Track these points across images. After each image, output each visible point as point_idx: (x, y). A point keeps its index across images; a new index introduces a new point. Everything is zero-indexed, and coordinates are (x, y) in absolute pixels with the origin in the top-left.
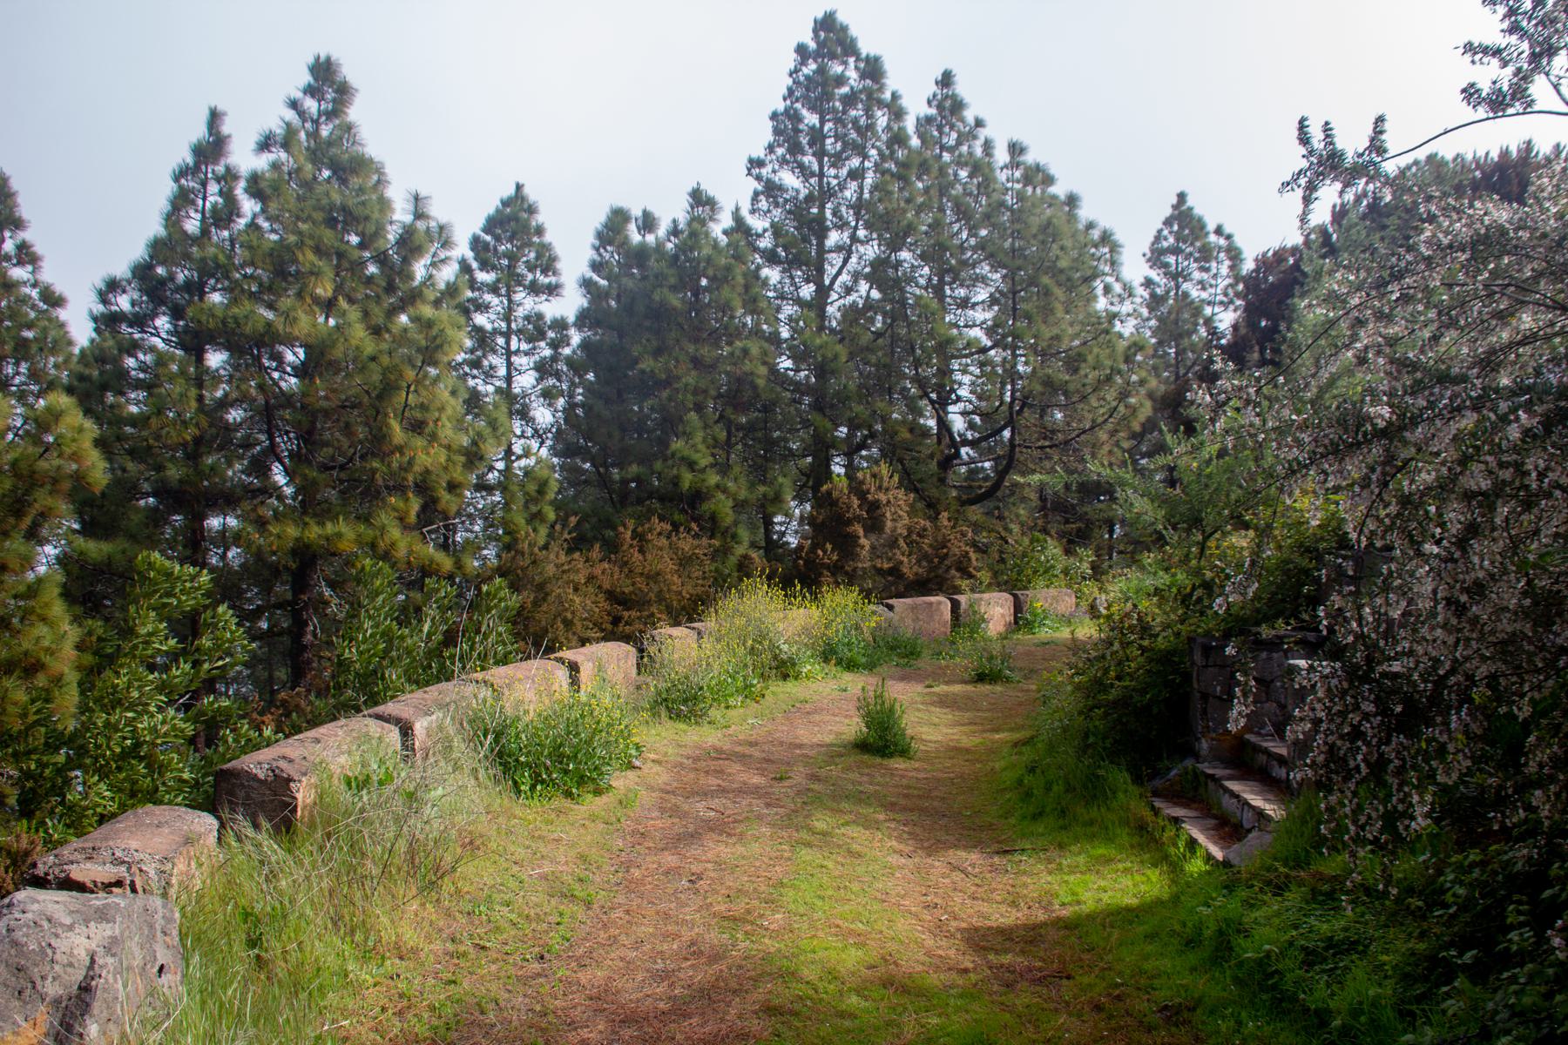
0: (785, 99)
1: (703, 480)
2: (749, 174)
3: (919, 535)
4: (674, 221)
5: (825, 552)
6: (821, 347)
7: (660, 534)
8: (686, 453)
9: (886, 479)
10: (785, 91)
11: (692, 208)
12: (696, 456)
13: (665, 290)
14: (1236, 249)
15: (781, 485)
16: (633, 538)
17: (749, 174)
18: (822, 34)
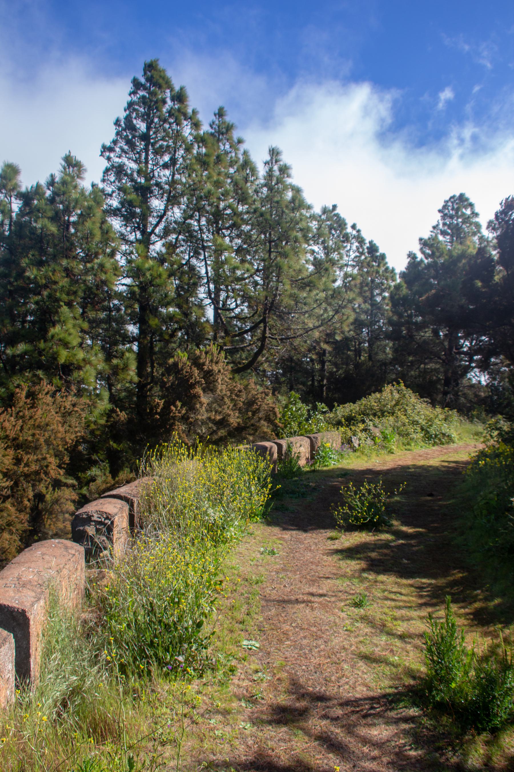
0: (125, 110)
1: (75, 355)
2: (102, 155)
3: (237, 395)
4: (52, 176)
5: (176, 407)
6: (149, 269)
7: (47, 393)
8: (62, 336)
9: (215, 355)
10: (126, 105)
11: (65, 168)
12: (69, 339)
13: (46, 221)
14: (362, 238)
15: (128, 359)
16: (27, 397)
17: (102, 155)
18: (149, 74)
